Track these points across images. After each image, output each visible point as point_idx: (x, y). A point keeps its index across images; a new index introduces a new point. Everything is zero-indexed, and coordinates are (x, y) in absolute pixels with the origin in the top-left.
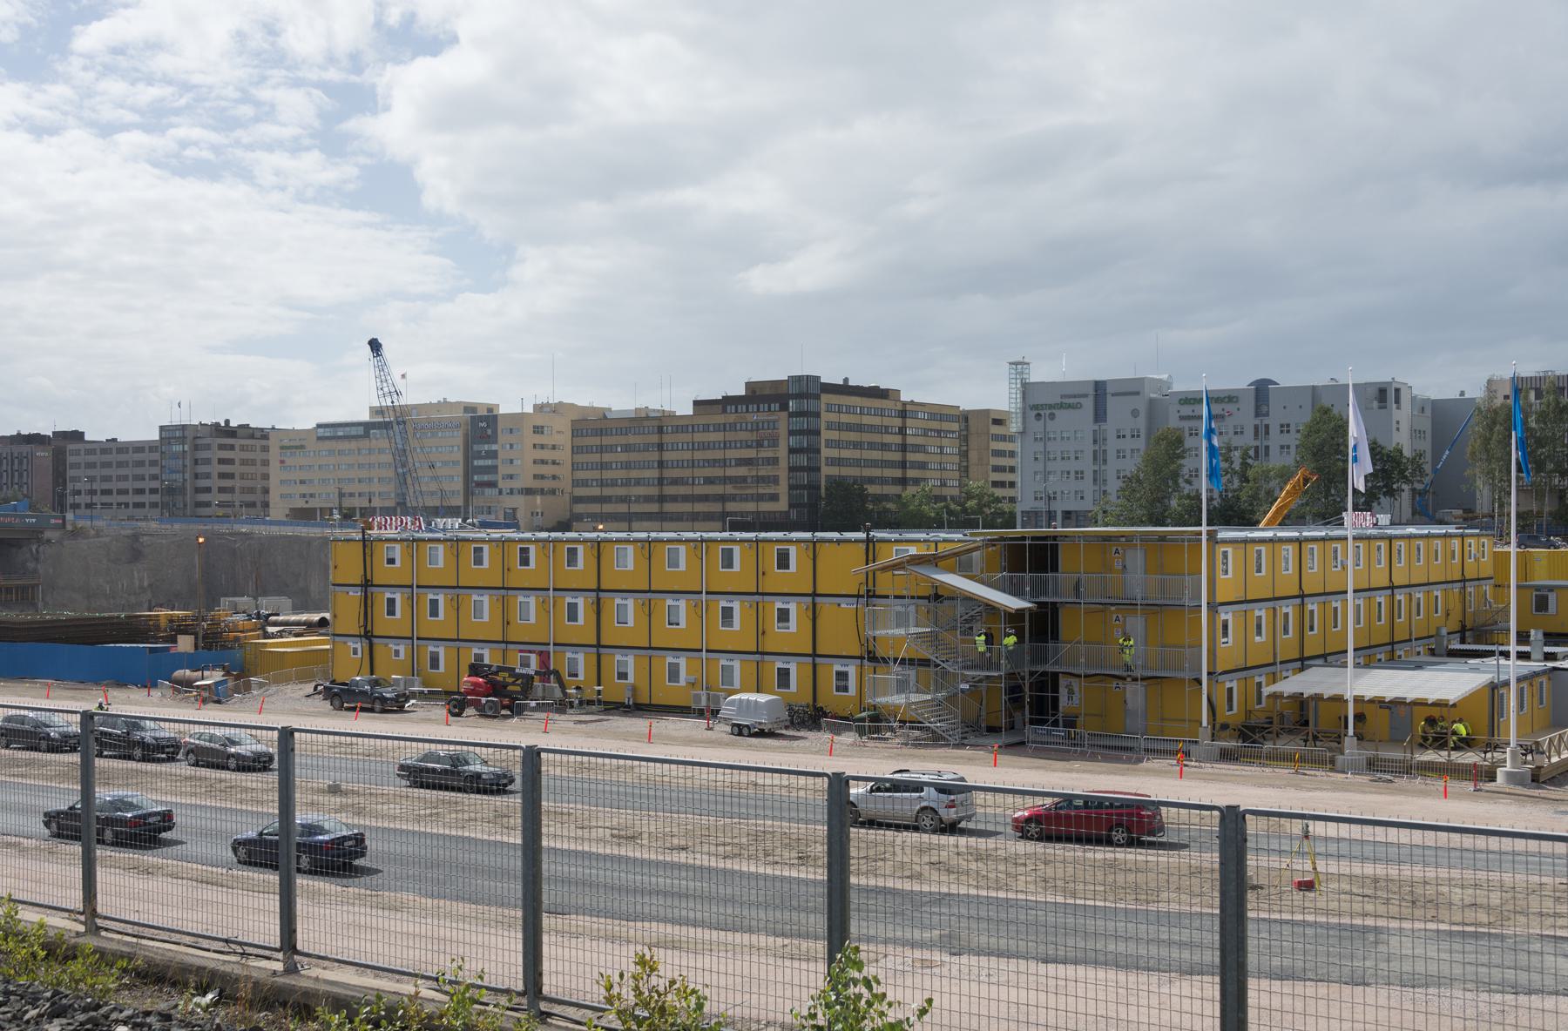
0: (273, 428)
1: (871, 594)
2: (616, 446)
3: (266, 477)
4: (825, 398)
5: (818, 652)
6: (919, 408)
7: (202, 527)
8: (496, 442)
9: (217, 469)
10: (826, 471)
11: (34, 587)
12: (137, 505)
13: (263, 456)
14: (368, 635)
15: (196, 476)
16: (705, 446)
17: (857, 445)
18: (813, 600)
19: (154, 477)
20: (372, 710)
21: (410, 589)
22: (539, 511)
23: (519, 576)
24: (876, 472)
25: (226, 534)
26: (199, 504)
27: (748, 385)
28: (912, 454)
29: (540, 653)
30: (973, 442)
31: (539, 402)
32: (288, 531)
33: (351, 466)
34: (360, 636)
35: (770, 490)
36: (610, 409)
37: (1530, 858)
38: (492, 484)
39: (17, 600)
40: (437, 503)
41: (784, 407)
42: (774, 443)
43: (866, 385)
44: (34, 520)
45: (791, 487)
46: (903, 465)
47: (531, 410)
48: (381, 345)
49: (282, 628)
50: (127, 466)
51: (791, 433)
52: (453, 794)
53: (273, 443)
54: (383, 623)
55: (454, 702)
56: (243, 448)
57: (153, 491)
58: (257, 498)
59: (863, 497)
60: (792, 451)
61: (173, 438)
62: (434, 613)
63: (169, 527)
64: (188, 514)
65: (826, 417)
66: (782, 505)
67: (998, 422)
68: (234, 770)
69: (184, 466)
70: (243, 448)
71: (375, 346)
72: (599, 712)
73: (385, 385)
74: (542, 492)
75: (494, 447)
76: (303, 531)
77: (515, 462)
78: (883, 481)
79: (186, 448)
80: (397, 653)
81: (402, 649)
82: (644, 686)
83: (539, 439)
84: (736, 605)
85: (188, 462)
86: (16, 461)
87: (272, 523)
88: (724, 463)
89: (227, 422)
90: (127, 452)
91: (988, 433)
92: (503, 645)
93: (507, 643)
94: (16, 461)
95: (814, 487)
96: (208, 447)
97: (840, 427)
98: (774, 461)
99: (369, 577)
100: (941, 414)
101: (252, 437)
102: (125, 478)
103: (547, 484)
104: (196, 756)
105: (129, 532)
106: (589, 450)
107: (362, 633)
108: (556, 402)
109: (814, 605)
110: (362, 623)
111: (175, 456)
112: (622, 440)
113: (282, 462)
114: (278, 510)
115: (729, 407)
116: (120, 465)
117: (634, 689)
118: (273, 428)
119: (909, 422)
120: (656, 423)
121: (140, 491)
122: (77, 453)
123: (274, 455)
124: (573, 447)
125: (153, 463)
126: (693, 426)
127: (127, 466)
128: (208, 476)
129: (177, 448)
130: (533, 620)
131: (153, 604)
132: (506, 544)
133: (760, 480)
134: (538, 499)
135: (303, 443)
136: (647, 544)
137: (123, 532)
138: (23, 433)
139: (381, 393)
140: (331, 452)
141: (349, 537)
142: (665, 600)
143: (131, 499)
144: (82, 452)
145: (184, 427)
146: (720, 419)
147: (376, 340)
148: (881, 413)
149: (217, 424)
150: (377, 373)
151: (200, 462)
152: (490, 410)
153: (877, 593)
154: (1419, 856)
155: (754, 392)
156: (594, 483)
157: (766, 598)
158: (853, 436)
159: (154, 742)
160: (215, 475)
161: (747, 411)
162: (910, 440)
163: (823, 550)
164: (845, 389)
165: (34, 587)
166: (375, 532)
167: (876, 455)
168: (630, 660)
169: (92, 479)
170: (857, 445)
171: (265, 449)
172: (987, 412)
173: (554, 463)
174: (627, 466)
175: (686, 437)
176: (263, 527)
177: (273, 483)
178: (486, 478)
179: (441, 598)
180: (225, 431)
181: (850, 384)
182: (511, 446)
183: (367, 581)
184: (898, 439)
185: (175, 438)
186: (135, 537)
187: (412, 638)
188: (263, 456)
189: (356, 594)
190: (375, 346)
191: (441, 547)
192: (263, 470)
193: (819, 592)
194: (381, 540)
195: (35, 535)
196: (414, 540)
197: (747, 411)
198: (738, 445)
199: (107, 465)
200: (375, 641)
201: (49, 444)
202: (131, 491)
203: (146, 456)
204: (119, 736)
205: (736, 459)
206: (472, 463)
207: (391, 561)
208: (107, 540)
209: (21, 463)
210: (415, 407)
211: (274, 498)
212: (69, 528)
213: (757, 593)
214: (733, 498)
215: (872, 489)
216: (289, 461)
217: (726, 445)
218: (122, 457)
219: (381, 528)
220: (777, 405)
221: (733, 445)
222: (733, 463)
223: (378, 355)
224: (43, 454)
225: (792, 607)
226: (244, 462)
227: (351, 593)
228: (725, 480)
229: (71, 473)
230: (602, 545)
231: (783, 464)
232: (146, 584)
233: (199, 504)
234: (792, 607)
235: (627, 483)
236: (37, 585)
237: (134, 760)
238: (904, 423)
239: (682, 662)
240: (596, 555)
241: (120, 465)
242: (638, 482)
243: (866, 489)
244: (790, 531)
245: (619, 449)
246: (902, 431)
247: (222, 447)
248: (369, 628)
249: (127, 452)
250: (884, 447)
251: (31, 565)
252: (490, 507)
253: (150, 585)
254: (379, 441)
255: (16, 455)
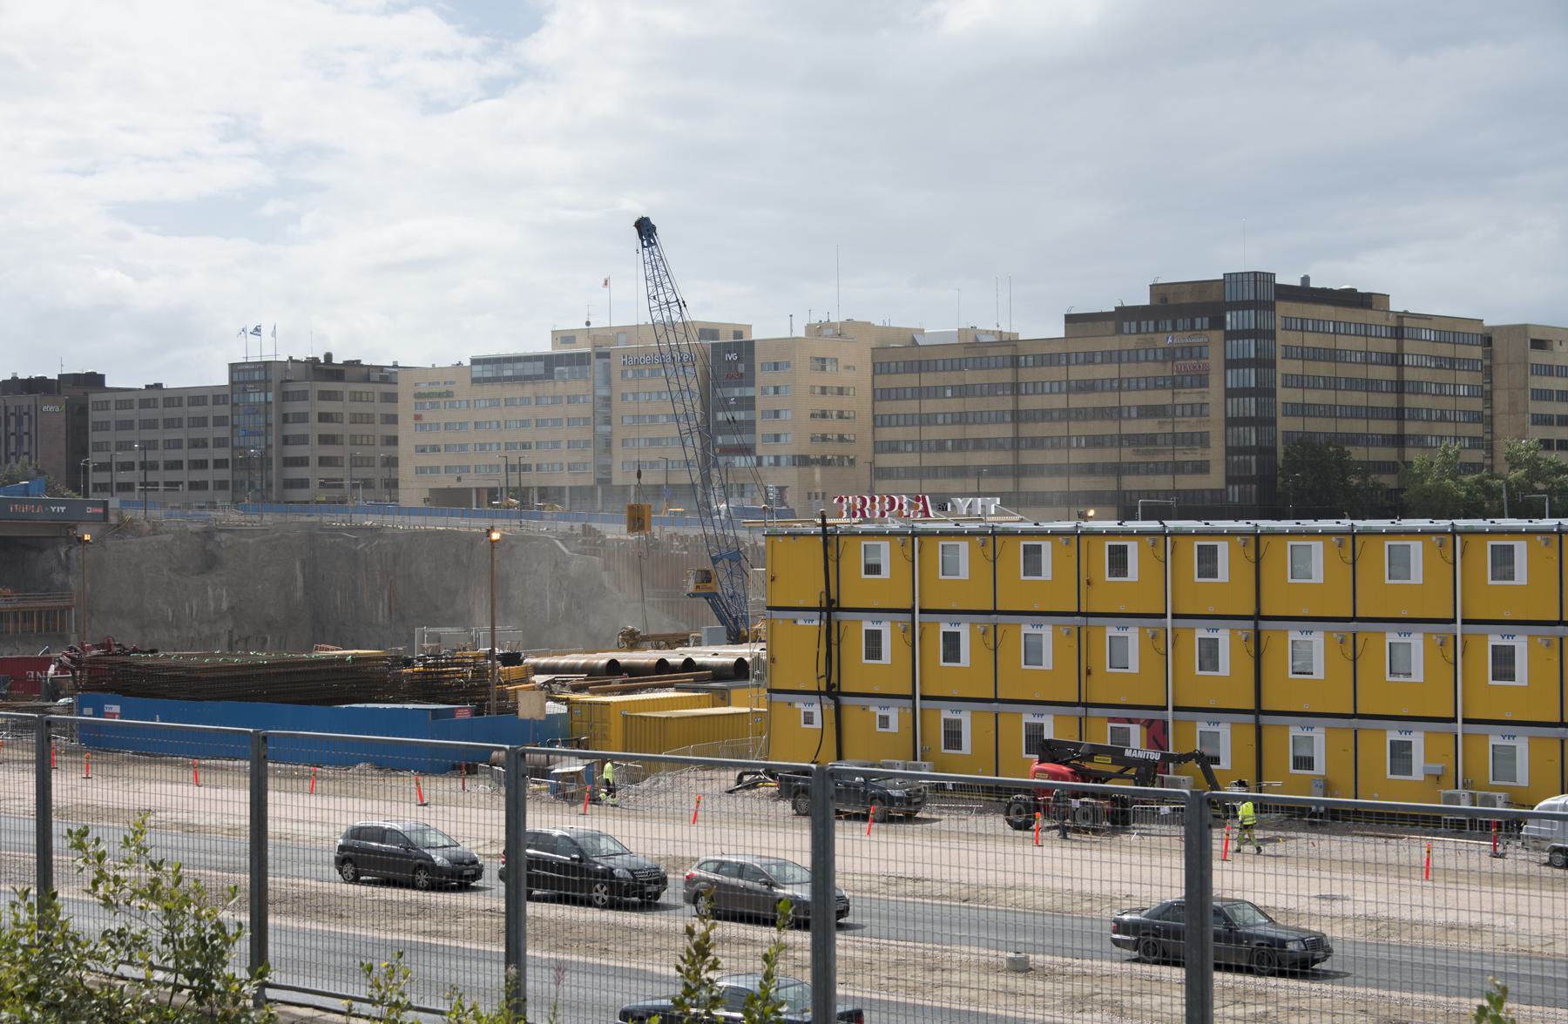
0: (395, 366)
1: (834, 606)
2: (944, 388)
3: (393, 441)
4: (1283, 308)
5: (1265, 707)
6: (1423, 323)
7: (305, 519)
8: (752, 384)
9: (315, 429)
10: (1285, 424)
11: (64, 610)
12: (194, 486)
13: (387, 408)
14: (833, 692)
15: (286, 440)
16: (1087, 387)
17: (1332, 384)
18: (1256, 625)
19: (219, 443)
20: (864, 818)
21: (909, 616)
22: (819, 490)
23: (1107, 591)
24: (1359, 426)
25: (341, 529)
26: (290, 484)
27: (1154, 288)
28: (1413, 397)
29: (1149, 724)
30: (1502, 377)
31: (815, 320)
32: (438, 524)
33: (524, 423)
34: (819, 693)
35: (1195, 456)
36: (921, 331)
37: (1473, 956)
38: (746, 450)
39: (39, 630)
40: (661, 480)
41: (1217, 323)
42: (1202, 381)
43: (1336, 288)
44: (63, 508)
45: (1229, 451)
46: (1399, 414)
47: (802, 334)
48: (654, 228)
49: (552, 677)
50: (180, 426)
51: (1230, 364)
52: (1239, 978)
53: (404, 390)
54: (857, 671)
55: (1017, 806)
56: (355, 397)
57: (220, 464)
58: (377, 473)
59: (1345, 467)
60: (1230, 393)
61: (249, 382)
62: (874, 651)
63: (256, 518)
64: (274, 498)
65: (1284, 338)
66: (1215, 479)
67: (1539, 344)
68: (603, 907)
69: (268, 425)
70: (355, 397)
71: (645, 228)
72: (1280, 826)
73: (660, 290)
74: (824, 462)
75: (749, 392)
76: (438, 524)
77: (783, 415)
78: (1366, 440)
79: (270, 397)
80: (884, 721)
81: (893, 714)
82: (1345, 777)
83: (820, 379)
84: (1520, 644)
85: (273, 418)
86: (13, 419)
87: (402, 511)
88: (1117, 413)
89: (328, 356)
90: (180, 405)
91: (1526, 363)
92: (1080, 710)
93: (1087, 705)
94: (13, 419)
95: (1265, 452)
96: (303, 396)
97: (1305, 354)
98: (1199, 410)
99: (833, 595)
100: (1452, 331)
101: (367, 379)
102: (177, 444)
103: (831, 451)
104: (355, 866)
105: (199, 527)
106: (899, 394)
107: (823, 688)
108: (843, 319)
109: (1258, 634)
110: (822, 671)
111: (253, 410)
112: (954, 378)
113: (418, 417)
114: (412, 491)
115: (1126, 325)
116: (170, 423)
117: (1327, 787)
118: (395, 366)
119: (1408, 346)
120: (1008, 351)
121: (200, 465)
122: (104, 406)
123: (405, 408)
124: (874, 391)
125: (220, 421)
126: (1068, 355)
127: (180, 426)
128: (303, 440)
129: (256, 397)
130: (1134, 666)
131: (235, 638)
132: (1082, 539)
133: (1177, 440)
134: (818, 472)
135: (449, 388)
136: (1349, 539)
137: (191, 527)
138: (20, 377)
139: (653, 303)
140: (494, 403)
141: (792, 530)
142: (1019, 625)
143: (185, 475)
144: (112, 405)
145: (266, 366)
146: (1112, 343)
147: (647, 219)
148: (1365, 331)
149: (316, 360)
150: (649, 272)
151: (290, 419)
152: (738, 334)
153: (842, 605)
154: (1452, 958)
155: (1164, 300)
156: (909, 447)
157: (1092, 621)
158: (1323, 369)
159: (628, 875)
160: (314, 439)
161: (1157, 330)
162: (1409, 374)
163: (1270, 547)
164: (1305, 293)
165: (64, 610)
166: (843, 522)
167: (1357, 398)
168: (1319, 735)
169: (148, 446)
170: (1332, 384)
171: (391, 398)
172: (1524, 328)
173: (841, 415)
174: (961, 419)
175: (1057, 373)
176: (398, 519)
177: (405, 449)
178: (735, 440)
179: (964, 631)
180: (324, 371)
181: (1312, 285)
182: (777, 390)
183: (830, 601)
184: (1389, 373)
185: (255, 382)
186: (208, 534)
187: (912, 697)
188: (387, 408)
189: (812, 623)
190: (645, 228)
191: (964, 546)
192: (388, 430)
193: (1265, 612)
194: (856, 534)
195: (65, 532)
196: (914, 535)
197: (1157, 330)
198: (1143, 385)
199: (150, 424)
200: (845, 700)
201: (59, 392)
202: (185, 465)
203: (210, 410)
204: (566, 865)
205: (1139, 407)
206: (715, 417)
207: (873, 569)
208: (168, 538)
209: (19, 422)
210: (624, 330)
211: (405, 472)
212: (113, 520)
213: (1079, 614)
214: (1134, 469)
215: (1358, 454)
216: (429, 417)
217: (1120, 385)
218: (171, 412)
219: (854, 515)
220: (1206, 320)
221: (1134, 384)
222: (1134, 413)
223: (650, 244)
224: (52, 408)
225: (1223, 636)
226: (356, 419)
227: (801, 622)
228: (1121, 440)
229: (94, 437)
230: (1263, 540)
231: (1216, 413)
232: (225, 606)
233: (290, 484)
234: (1223, 636)
235: (960, 445)
236: (69, 608)
237: (597, 906)
238: (1400, 347)
239: (1417, 739)
240: (1253, 557)
241: (170, 423)
242: (979, 444)
243: (1349, 453)
244: (1403, 517)
245: (949, 393)
246: (1396, 360)
247: (325, 396)
248: (834, 679)
249: (180, 405)
250: (1369, 385)
251: (58, 578)
252: (743, 485)
253: (232, 608)
254: (565, 385)
255: (13, 411)
